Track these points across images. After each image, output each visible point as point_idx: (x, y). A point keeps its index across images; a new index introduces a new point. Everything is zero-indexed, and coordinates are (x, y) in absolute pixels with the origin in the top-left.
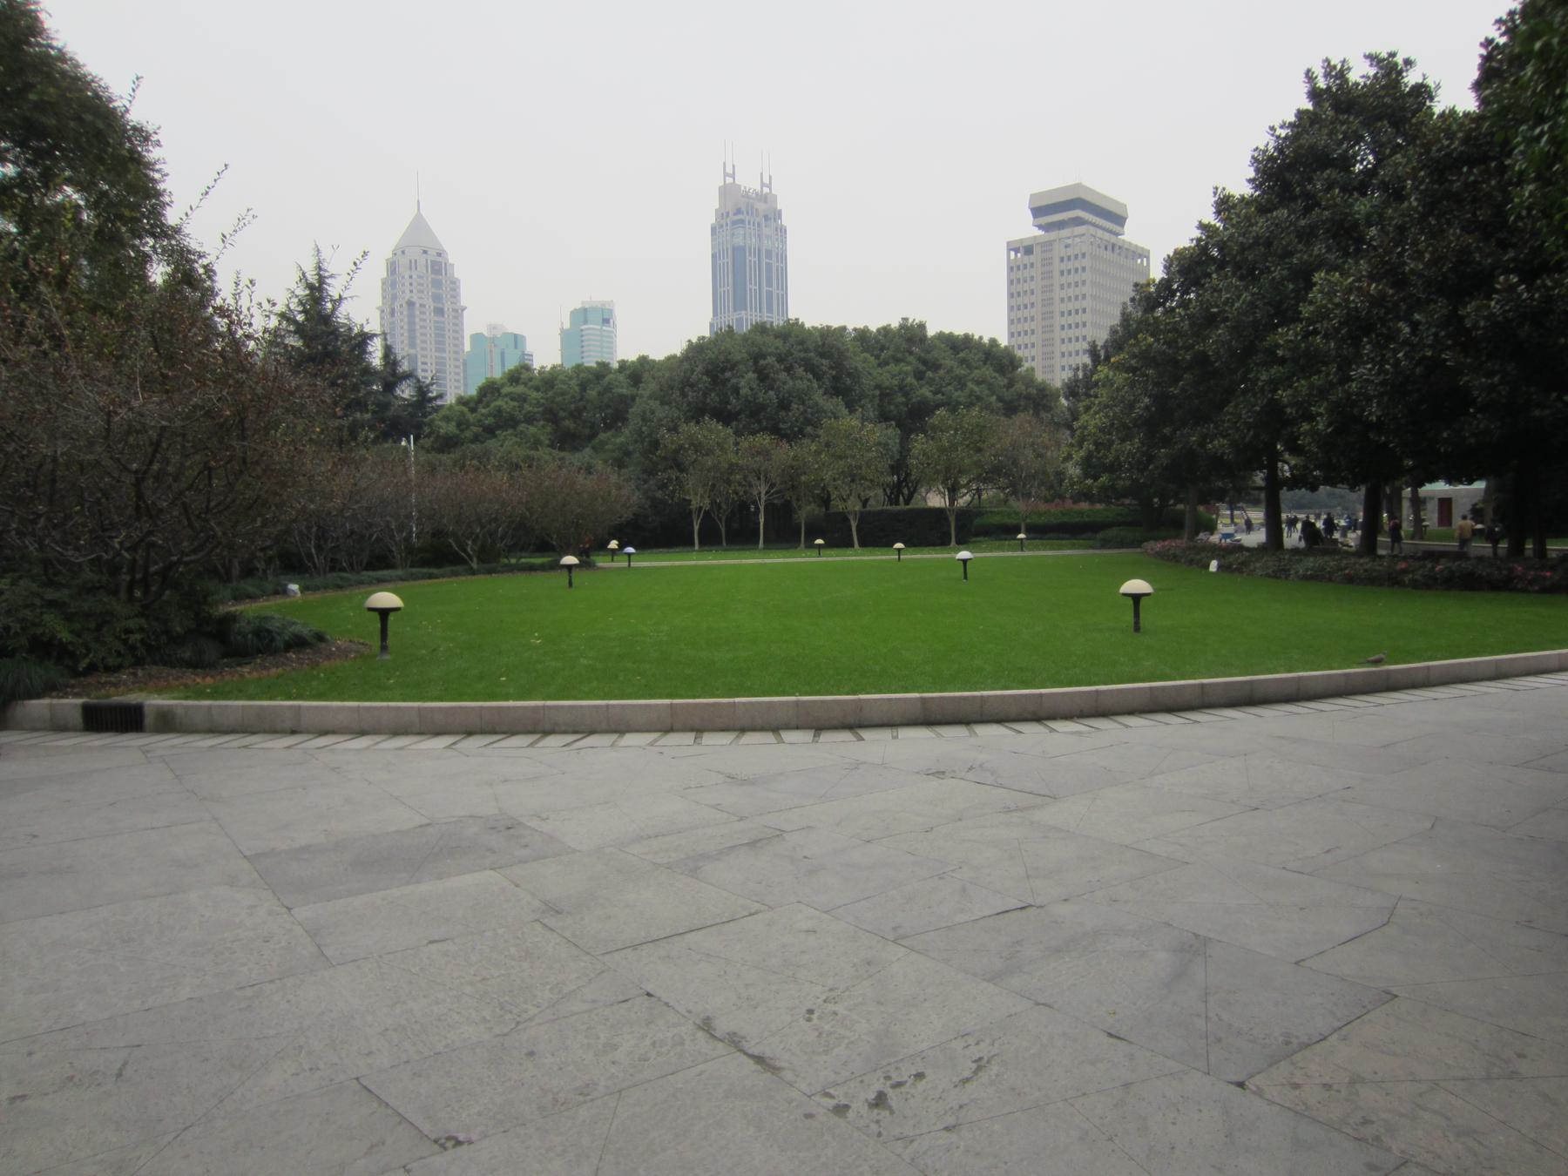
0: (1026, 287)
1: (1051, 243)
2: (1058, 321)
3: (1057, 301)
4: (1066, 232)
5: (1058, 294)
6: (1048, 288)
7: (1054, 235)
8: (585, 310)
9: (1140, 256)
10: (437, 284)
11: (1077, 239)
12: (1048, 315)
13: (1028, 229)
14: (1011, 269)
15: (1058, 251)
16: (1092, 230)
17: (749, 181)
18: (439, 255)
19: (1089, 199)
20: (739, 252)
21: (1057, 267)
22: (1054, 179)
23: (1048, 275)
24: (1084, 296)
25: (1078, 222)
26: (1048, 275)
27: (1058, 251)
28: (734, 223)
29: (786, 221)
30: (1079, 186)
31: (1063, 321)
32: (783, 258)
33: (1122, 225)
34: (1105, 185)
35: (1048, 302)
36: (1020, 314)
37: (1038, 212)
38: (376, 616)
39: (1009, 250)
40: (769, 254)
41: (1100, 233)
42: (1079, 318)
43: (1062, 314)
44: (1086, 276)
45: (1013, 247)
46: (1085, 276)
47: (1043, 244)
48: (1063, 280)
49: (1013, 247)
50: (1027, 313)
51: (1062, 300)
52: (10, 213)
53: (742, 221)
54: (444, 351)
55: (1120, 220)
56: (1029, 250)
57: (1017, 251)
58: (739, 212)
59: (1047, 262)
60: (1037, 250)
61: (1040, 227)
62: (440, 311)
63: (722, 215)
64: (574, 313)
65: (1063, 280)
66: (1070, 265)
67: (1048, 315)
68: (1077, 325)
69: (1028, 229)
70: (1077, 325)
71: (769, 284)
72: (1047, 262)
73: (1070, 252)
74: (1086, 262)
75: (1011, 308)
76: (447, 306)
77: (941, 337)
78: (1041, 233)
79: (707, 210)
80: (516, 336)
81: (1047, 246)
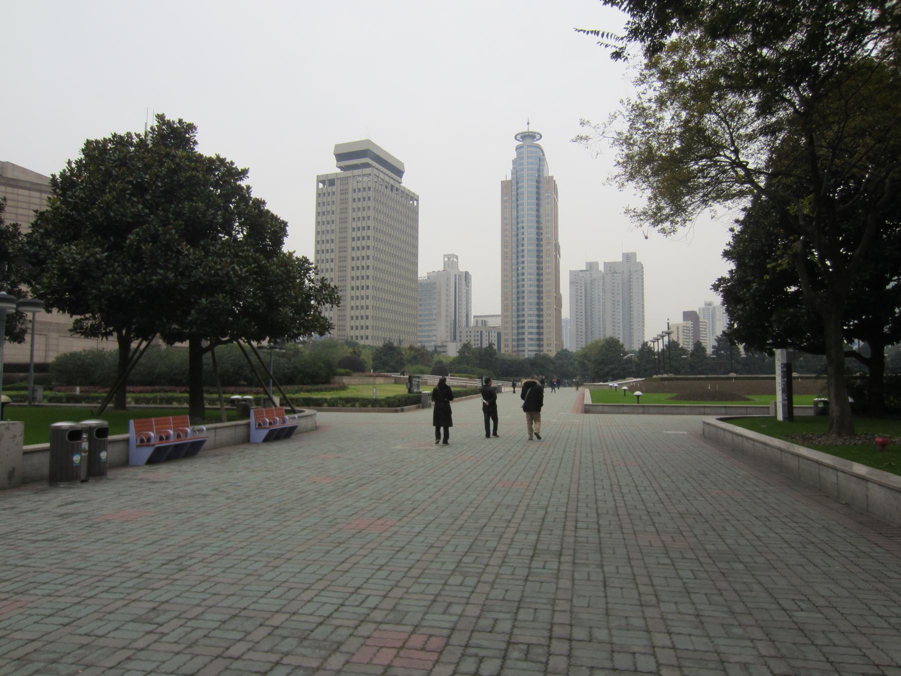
0: (329, 199)
1: (347, 178)
2: (351, 234)
3: (350, 219)
4: (357, 172)
5: (350, 215)
6: (344, 211)
7: (349, 173)
11: (364, 178)
12: (344, 230)
13: (332, 168)
14: (319, 195)
15: (352, 184)
16: (376, 172)
17: (639, 195)
19: (375, 151)
21: (351, 195)
22: (352, 136)
23: (344, 201)
24: (368, 247)
25: (367, 165)
26: (344, 201)
27: (352, 184)
30: (368, 142)
31: (354, 264)
34: (390, 145)
35: (344, 220)
36: (324, 228)
37: (340, 157)
41: (382, 175)
42: (363, 283)
43: (353, 239)
44: (371, 203)
45: (321, 180)
46: (370, 203)
47: (342, 179)
48: (355, 205)
49: (321, 180)
50: (328, 246)
51: (353, 278)
56: (332, 182)
57: (323, 182)
59: (344, 192)
60: (337, 183)
61: (341, 168)
65: (353, 303)
66: (360, 195)
67: (344, 230)
68: (357, 298)
69: (332, 168)
70: (357, 298)
72: (344, 192)
73: (360, 186)
74: (371, 194)
75: (318, 223)
77: (268, 212)
78: (339, 171)
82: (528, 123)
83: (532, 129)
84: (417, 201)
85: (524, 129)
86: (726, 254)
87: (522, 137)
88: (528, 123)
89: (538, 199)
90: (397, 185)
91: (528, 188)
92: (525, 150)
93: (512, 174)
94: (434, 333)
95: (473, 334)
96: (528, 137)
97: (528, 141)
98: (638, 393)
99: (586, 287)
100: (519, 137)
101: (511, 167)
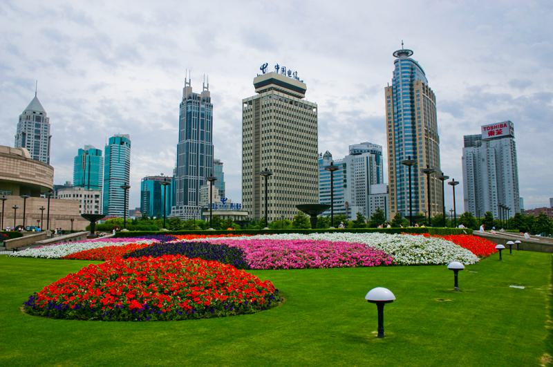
8: (115, 138)
9: (314, 108)
10: (38, 126)
13: (252, 93)
15: (263, 102)
17: (197, 90)
18: (41, 114)
20: (189, 115)
27: (263, 102)
28: (188, 102)
29: (212, 102)
32: (211, 118)
33: (304, 93)
37: (257, 85)
38: (375, 306)
39: (243, 103)
40: (203, 115)
41: (281, 94)
52: (175, 174)
53: (191, 102)
54: (38, 154)
55: (303, 91)
56: (250, 103)
58: (190, 98)
61: (257, 92)
62: (38, 137)
63: (184, 99)
64: (110, 139)
69: (252, 93)
71: (202, 128)
76: (42, 135)
79: (463, 138)
80: (97, 150)
81: (257, 100)
82: (402, 44)
83: (406, 47)
84: (316, 108)
85: (400, 48)
86: (48, 118)
87: (398, 54)
88: (402, 44)
89: (412, 98)
90: (301, 100)
91: (403, 91)
92: (399, 63)
93: (393, 81)
94: (342, 196)
95: (379, 199)
96: (403, 53)
97: (404, 57)
98: (461, 227)
99: (474, 157)
100: (396, 54)
101: (392, 76)
